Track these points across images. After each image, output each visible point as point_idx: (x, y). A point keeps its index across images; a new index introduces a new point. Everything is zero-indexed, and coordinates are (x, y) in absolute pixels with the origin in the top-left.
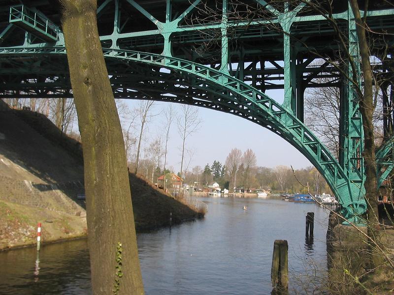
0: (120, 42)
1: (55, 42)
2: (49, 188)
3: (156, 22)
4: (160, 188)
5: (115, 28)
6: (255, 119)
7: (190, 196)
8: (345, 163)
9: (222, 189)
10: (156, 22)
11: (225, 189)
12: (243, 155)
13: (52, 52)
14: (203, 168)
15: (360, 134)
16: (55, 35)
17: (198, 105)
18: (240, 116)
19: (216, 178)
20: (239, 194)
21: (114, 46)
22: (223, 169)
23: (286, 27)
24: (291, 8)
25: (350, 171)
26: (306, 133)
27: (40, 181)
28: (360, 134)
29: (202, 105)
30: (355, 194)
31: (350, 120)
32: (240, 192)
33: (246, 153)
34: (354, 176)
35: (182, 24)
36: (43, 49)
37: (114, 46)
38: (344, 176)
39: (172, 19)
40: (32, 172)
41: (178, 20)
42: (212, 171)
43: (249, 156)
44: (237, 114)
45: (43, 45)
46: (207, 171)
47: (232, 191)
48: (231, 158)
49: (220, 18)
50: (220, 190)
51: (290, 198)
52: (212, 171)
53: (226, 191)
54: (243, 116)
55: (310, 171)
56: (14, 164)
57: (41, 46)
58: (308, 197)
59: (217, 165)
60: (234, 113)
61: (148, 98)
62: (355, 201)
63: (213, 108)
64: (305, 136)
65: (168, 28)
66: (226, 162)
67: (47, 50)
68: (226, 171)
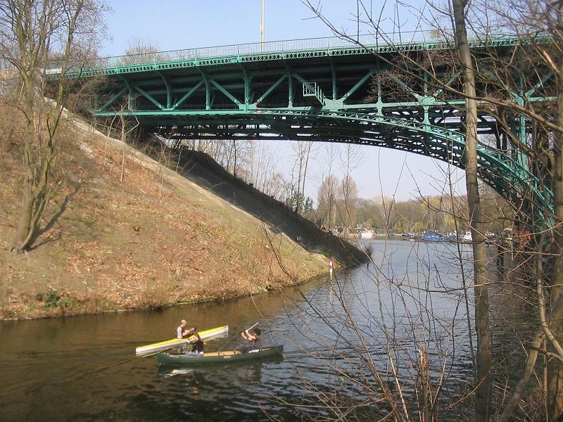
3: (417, 96)
5: (290, 102)
6: (437, 155)
10: (417, 96)
12: (340, 184)
17: (365, 144)
23: (290, 107)
29: (368, 144)
35: (346, 102)
36: (310, 112)
37: (380, 113)
39: (338, 98)
41: (344, 99)
43: (348, 186)
51: (415, 238)
54: (409, 151)
65: (427, 101)
66: (319, 193)
68: (311, 204)
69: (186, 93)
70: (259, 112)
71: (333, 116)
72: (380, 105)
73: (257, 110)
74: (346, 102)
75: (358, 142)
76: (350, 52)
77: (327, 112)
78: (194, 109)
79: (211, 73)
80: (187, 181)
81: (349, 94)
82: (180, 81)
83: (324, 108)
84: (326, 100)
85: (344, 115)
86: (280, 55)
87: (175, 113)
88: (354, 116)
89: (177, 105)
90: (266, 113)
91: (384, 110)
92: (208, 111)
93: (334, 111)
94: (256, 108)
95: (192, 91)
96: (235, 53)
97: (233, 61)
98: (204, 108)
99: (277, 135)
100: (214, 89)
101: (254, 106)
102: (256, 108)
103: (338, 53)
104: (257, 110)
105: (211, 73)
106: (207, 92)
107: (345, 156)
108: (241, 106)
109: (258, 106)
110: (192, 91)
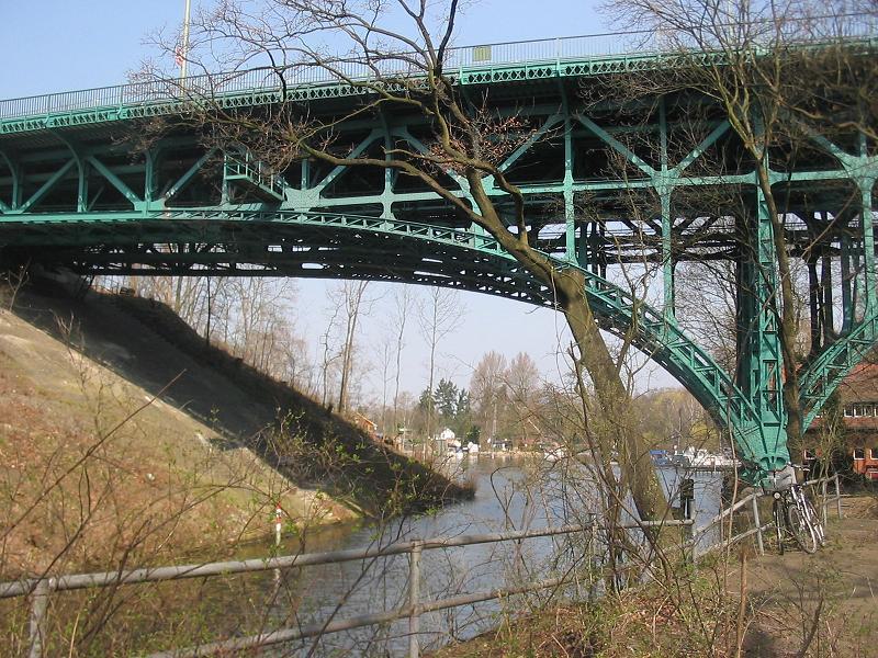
0: (395, 205)
1: (280, 202)
2: (235, 446)
4: (386, 442)
7: (452, 455)
8: (753, 394)
9: (465, 444)
11: (471, 443)
12: (508, 366)
13: (275, 220)
14: (417, 398)
15: (776, 355)
16: (280, 192)
17: (423, 283)
18: (498, 294)
19: (447, 418)
20: (503, 454)
21: (387, 214)
22: (461, 398)
24: (676, 159)
25: (763, 408)
26: (698, 356)
27: (215, 434)
28: (776, 355)
30: (770, 443)
31: (761, 335)
32: (504, 449)
33: (517, 362)
34: (769, 417)
36: (258, 214)
37: (387, 214)
38: (751, 414)
39: (310, 185)
40: (195, 417)
41: (321, 187)
42: (436, 403)
44: (492, 293)
45: (257, 207)
46: (425, 404)
47: (484, 447)
48: (481, 376)
49: (562, 176)
50: (458, 444)
52: (436, 403)
53: (473, 447)
54: (503, 295)
55: (655, 400)
56: (168, 406)
57: (252, 209)
58: (660, 456)
59: (446, 389)
60: (486, 292)
61: (362, 278)
62: (771, 454)
63: (514, 298)
64: (696, 359)
67: (266, 216)
68: (468, 402)
69: (44, 183)
70: (168, 216)
71: (302, 220)
72: (387, 198)
73: (163, 212)
74: (325, 193)
75: (410, 278)
76: (540, 72)
77: (290, 213)
78: (52, 211)
79: (92, 143)
80: (136, 387)
81: (330, 179)
82: (36, 158)
83: (285, 206)
84: (289, 191)
85: (319, 219)
86: (553, 68)
87: (26, 219)
88: (339, 221)
89: (28, 204)
90: (180, 217)
91: (582, 204)
92: (83, 215)
93: (302, 210)
94: (162, 208)
95: (54, 178)
96: (116, 102)
97: (112, 117)
98: (74, 210)
99: (261, 267)
100: (582, 133)
101: (159, 204)
102: (162, 208)
103: (480, 78)
104: (163, 212)
105: (92, 143)
106: (15, 185)
107: (429, 308)
108: (138, 205)
109: (166, 204)
110: (54, 178)
